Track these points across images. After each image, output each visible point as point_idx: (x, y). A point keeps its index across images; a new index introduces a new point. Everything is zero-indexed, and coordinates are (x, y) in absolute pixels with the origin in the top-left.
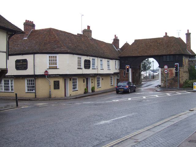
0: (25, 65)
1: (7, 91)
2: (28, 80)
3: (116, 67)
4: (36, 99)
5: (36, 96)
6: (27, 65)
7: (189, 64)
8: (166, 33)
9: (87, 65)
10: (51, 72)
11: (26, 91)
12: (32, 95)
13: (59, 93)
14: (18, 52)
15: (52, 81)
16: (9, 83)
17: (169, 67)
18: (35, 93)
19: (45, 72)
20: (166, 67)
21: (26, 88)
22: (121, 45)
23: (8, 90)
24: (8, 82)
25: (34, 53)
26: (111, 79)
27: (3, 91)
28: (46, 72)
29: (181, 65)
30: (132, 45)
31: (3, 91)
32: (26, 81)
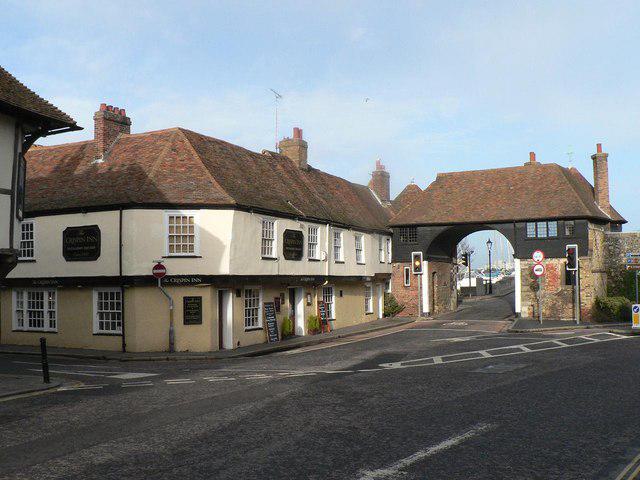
0: (91, 244)
1: (37, 329)
2: (100, 294)
3: (358, 258)
4: (126, 358)
5: (124, 345)
6: (98, 244)
7: (606, 248)
8: (533, 155)
9: (294, 246)
10: (174, 268)
11: (96, 329)
12: (114, 344)
13: (196, 339)
14: (73, 204)
15: (178, 295)
16: (42, 303)
17: (546, 257)
18: (123, 335)
19: (156, 268)
20: (538, 255)
21: (96, 319)
22: (395, 192)
23: (40, 323)
24: (40, 300)
25: (121, 206)
26: (380, 241)
27: (26, 327)
28: (159, 266)
29: (585, 251)
30: (428, 189)
31: (26, 327)
32: (95, 296)
